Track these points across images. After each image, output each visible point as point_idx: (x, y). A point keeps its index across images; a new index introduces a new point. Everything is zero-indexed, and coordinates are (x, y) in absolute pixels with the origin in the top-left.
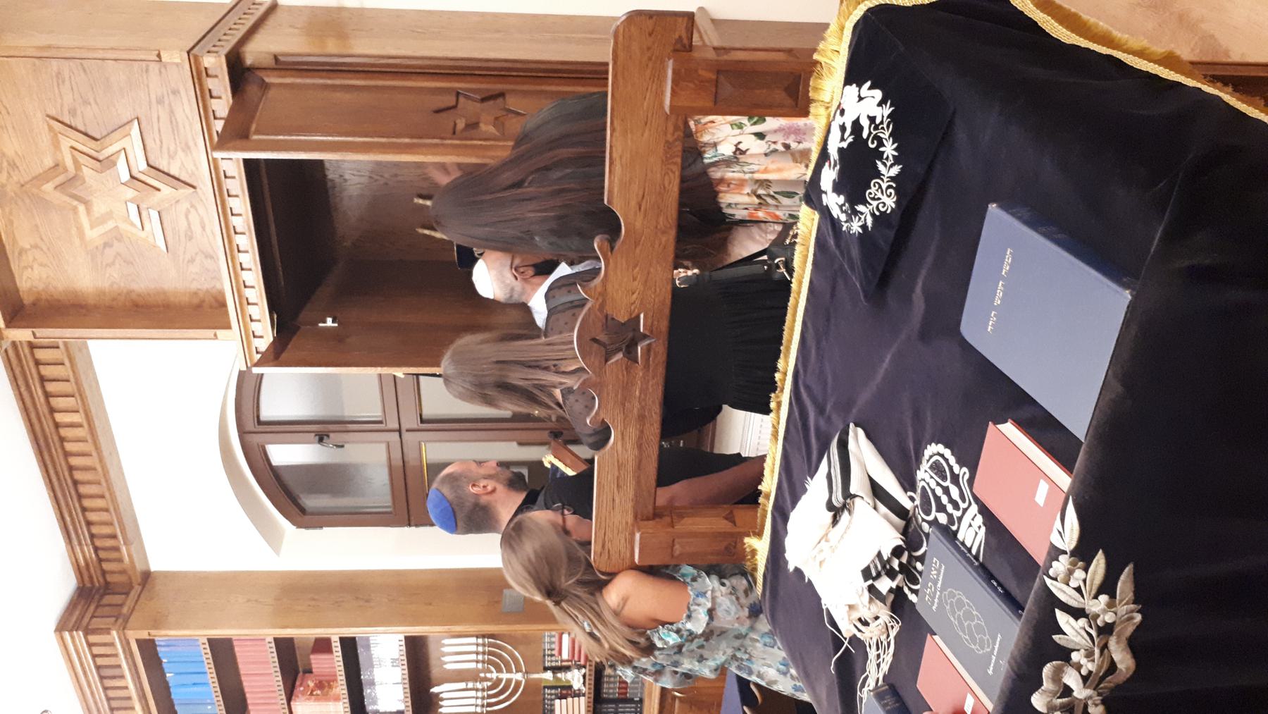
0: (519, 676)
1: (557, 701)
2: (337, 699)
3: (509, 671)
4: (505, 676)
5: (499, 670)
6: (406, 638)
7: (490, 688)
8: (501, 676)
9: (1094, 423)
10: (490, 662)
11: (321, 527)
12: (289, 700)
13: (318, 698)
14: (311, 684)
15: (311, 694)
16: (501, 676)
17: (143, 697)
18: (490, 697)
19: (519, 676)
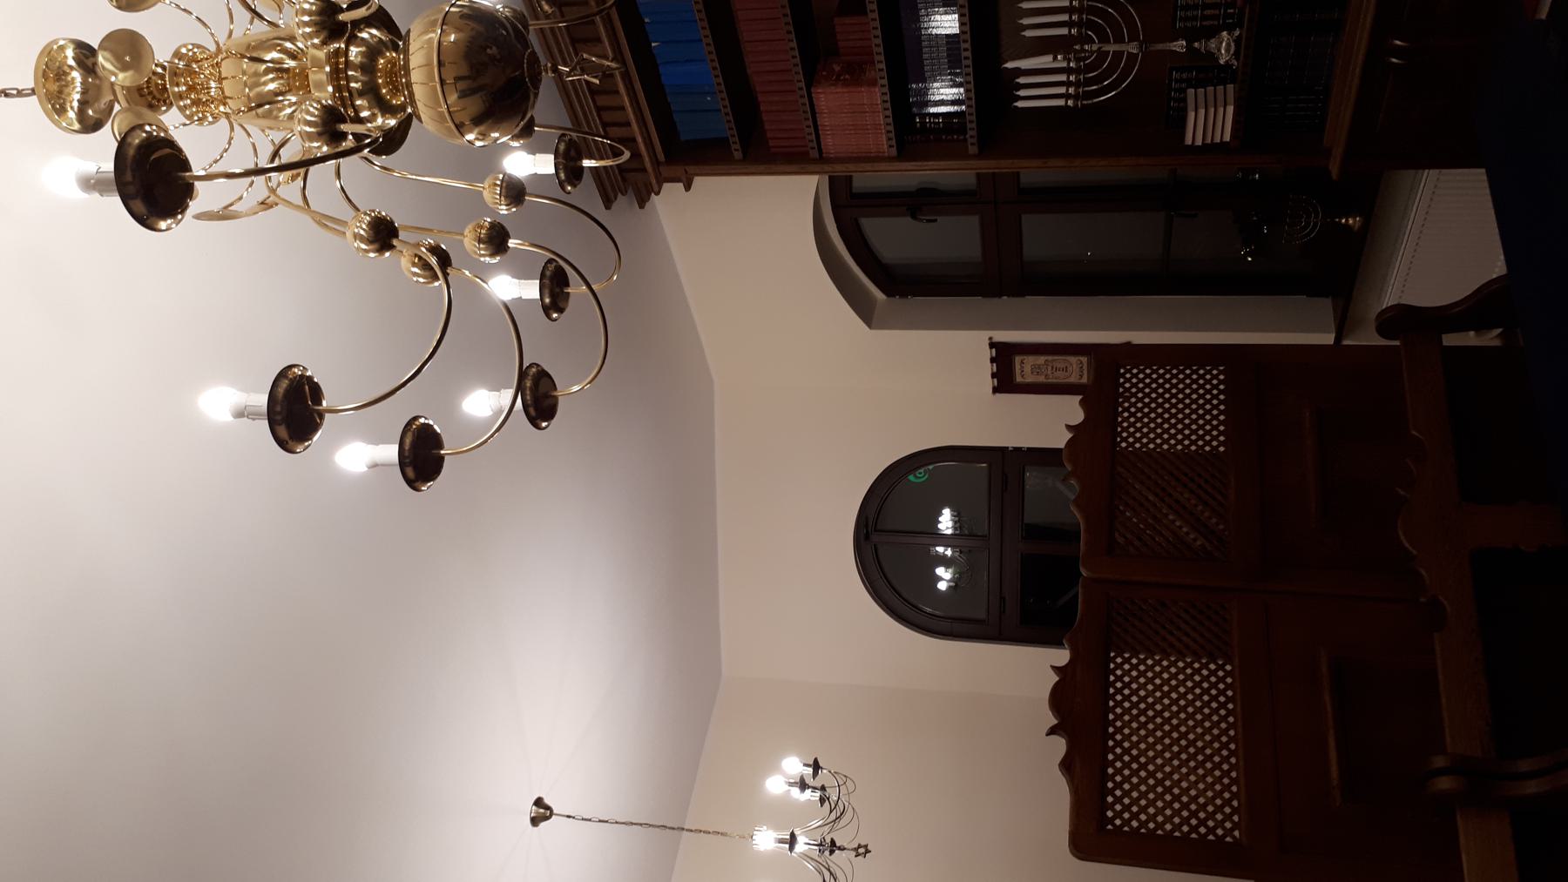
0: (1133, 48)
1: (1191, 91)
2: (873, 83)
3: (1119, 39)
4: (1112, 48)
5: (1104, 39)
6: (978, 175)
7: (1089, 68)
8: (1106, 48)
9: (762, 168)
10: (1091, 25)
11: (1000, 296)
12: (809, 86)
13: (846, 84)
14: (837, 68)
15: (838, 79)
16: (1106, 48)
17: (626, 76)
18: (1089, 82)
19: (1133, 48)
